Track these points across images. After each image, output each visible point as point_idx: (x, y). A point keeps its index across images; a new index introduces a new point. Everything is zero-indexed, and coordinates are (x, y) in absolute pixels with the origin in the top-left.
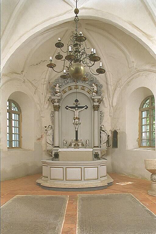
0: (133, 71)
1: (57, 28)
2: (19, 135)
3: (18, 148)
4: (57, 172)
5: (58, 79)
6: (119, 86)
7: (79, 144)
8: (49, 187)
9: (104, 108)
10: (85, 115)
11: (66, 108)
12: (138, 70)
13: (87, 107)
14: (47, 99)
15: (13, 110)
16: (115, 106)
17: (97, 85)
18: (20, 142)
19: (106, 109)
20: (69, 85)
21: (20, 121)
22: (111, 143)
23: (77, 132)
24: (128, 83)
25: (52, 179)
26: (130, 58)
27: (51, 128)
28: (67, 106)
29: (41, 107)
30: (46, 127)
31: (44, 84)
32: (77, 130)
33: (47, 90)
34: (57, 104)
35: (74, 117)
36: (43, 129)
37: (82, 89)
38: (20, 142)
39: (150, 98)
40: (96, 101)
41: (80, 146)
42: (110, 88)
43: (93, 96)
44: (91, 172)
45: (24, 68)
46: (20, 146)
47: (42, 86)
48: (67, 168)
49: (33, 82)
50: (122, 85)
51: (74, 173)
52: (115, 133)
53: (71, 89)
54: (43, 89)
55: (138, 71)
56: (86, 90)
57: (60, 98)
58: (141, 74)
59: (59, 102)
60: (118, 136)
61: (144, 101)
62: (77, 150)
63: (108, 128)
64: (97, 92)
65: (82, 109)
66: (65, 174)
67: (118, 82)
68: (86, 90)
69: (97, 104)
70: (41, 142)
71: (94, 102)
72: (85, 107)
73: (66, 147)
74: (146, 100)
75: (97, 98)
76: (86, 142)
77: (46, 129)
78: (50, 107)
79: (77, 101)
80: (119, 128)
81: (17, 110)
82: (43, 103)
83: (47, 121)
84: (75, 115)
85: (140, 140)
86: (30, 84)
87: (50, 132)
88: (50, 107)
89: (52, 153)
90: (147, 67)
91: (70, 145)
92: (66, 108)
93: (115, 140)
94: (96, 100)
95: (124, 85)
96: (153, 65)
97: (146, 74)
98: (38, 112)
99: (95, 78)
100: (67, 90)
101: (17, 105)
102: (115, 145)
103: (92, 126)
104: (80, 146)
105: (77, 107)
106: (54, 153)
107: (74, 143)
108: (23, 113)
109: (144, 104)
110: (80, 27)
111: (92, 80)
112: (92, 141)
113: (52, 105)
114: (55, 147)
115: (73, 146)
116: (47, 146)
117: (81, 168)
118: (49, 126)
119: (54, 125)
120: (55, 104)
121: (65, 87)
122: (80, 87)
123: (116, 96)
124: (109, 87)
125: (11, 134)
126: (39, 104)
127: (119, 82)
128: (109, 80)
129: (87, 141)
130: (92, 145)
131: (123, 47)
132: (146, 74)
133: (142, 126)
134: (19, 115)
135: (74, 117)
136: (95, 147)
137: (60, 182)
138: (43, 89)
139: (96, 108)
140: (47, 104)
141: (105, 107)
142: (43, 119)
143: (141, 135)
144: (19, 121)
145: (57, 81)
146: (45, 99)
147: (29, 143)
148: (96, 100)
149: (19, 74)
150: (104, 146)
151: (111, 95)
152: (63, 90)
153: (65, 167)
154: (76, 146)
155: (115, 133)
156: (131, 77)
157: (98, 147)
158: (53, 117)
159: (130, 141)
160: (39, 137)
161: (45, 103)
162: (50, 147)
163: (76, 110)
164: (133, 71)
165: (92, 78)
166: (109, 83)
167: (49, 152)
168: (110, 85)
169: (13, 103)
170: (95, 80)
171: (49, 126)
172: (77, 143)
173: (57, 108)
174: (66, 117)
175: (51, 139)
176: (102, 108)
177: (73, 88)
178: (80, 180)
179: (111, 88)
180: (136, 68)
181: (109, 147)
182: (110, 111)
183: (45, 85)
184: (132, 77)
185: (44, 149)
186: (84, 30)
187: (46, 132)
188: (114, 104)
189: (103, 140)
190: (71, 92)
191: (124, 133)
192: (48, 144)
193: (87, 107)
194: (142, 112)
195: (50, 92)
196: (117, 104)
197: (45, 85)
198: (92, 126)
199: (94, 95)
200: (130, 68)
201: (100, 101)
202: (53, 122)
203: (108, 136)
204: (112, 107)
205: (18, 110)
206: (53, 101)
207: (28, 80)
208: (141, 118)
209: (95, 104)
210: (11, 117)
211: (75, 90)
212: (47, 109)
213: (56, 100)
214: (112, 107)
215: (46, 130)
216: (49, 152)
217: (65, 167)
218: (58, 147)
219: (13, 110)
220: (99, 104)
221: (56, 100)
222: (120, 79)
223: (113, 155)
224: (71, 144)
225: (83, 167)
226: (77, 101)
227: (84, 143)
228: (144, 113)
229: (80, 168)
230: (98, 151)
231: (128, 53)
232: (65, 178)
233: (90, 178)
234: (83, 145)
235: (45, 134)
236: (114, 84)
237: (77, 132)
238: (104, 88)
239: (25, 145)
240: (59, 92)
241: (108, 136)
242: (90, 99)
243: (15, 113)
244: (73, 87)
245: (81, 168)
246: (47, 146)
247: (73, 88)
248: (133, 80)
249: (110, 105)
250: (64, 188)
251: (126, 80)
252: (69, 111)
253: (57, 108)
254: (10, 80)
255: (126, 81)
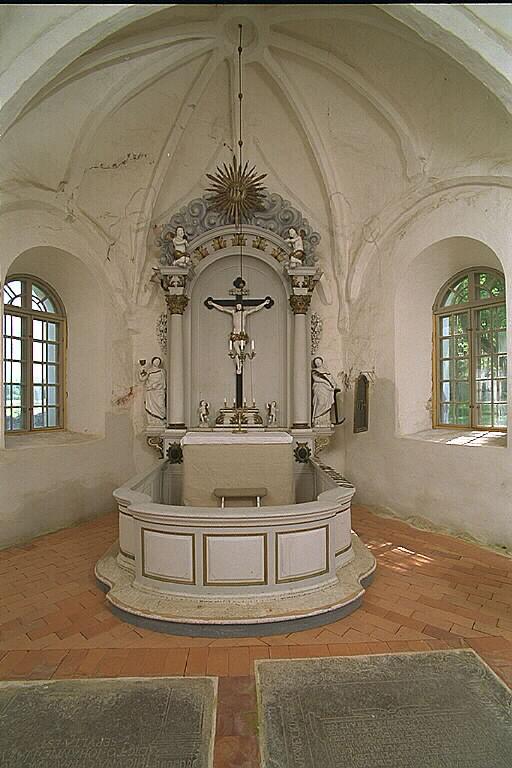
0: (420, 189)
1: (173, 40)
2: (58, 387)
3: (53, 428)
4: (170, 553)
5: (181, 215)
6: (371, 239)
7: (246, 415)
8: (136, 615)
9: (323, 306)
10: (266, 328)
11: (206, 303)
12: (441, 184)
13: (272, 302)
14: (146, 281)
15: (35, 307)
16: (359, 300)
17: (303, 235)
18: (60, 410)
19: (328, 308)
20: (217, 234)
21: (61, 344)
22: (348, 412)
23: (239, 378)
24: (402, 230)
25: (151, 577)
26: (414, 145)
27: (161, 365)
28: (210, 299)
29: (129, 301)
30: (143, 363)
31: (138, 231)
32: (239, 373)
33: (149, 248)
34: (179, 291)
35: (232, 334)
36: (134, 370)
37: (258, 248)
38: (60, 410)
39: (471, 275)
40: (301, 284)
41: (251, 422)
42: (342, 247)
43: (293, 268)
44: (303, 550)
45: (68, 172)
46: (61, 424)
47: (134, 235)
48: (209, 535)
49: (99, 222)
50: (382, 235)
51: (236, 554)
52: (363, 382)
53: (222, 244)
54: (136, 247)
55: (441, 187)
56: (270, 248)
57: (186, 272)
58: (449, 197)
59: (184, 285)
60: (370, 392)
61: (448, 283)
62: (240, 439)
63: (335, 361)
64: (303, 256)
65: (257, 308)
66: (202, 558)
67: (366, 226)
68: (270, 248)
69: (305, 292)
70: (129, 409)
71: (293, 286)
72: (263, 301)
73: (206, 425)
74: (456, 280)
75: (301, 272)
76: (270, 409)
77: (142, 368)
78: (156, 301)
79: (239, 283)
80: (371, 366)
81: (50, 310)
82: (135, 292)
83: (146, 344)
84: (234, 327)
85: (437, 405)
86: (92, 228)
87: (156, 378)
88: (156, 301)
89: (161, 444)
90: (477, 170)
91: (219, 420)
92: (206, 303)
93: (359, 406)
94: (301, 280)
95: (385, 236)
96: (500, 159)
97: (467, 195)
98: (120, 312)
99: (295, 214)
100: (209, 247)
101: (50, 293)
102: (361, 422)
103: (289, 359)
104: (251, 422)
105: (240, 302)
106: (167, 447)
107: (233, 415)
108: (73, 319)
109: (449, 292)
110: (253, 40)
111: (287, 220)
112: (289, 399)
113: (164, 293)
114: (172, 426)
115: (227, 422)
116: (146, 423)
117: (265, 535)
118: (155, 358)
119: (169, 358)
120: (173, 291)
121: (203, 239)
122: (249, 241)
123: (361, 268)
124: (340, 241)
125: (29, 388)
126: (121, 291)
127: (371, 226)
128: (339, 219)
129: (270, 406)
130: (289, 420)
131: (388, 109)
132: (467, 195)
133: (441, 362)
134: (58, 325)
135: (232, 334)
136: (295, 426)
137: (180, 593)
138: (134, 244)
139: (299, 305)
140: (148, 294)
141: (326, 303)
142: (134, 337)
143: (438, 387)
144: (58, 345)
145: (178, 221)
146: (141, 278)
147: (91, 413)
148: (301, 280)
149: (53, 190)
150: (324, 422)
151: (346, 260)
152: (198, 249)
153: (199, 534)
154: (239, 422)
155: (363, 382)
156: (411, 208)
157: (305, 426)
158: (165, 331)
159: (409, 405)
160: (122, 394)
161: (143, 289)
162: (156, 427)
163: (237, 311)
164: (420, 189)
165: (286, 212)
166: (339, 230)
167: (154, 442)
168: (342, 235)
169: (36, 285)
170: (296, 218)
171: (155, 358)
172: (239, 414)
173: (177, 305)
174: (209, 336)
175: (161, 402)
176: (315, 303)
177: (229, 243)
178: (261, 584)
179: (345, 245)
180: (431, 179)
181: (337, 423)
182: (342, 314)
183: (141, 234)
184: (412, 211)
185: (138, 430)
186: (267, 53)
187: (145, 378)
188: (355, 294)
189: (321, 403)
190: (221, 254)
191: (389, 385)
192: (149, 415)
193: (272, 302)
194: (441, 318)
195: (157, 255)
196: (364, 294)
197: (141, 234)
198: (289, 359)
199: (294, 265)
200: (409, 180)
201: (311, 283)
202: (166, 345)
203: (336, 391)
204: (349, 301)
205: (56, 310)
206: (165, 283)
207: (84, 214)
208: (438, 339)
209: (298, 292)
210: (29, 331)
211: (237, 250)
212: (148, 309)
213: (176, 279)
214: (349, 301)
215: (144, 372)
216: (154, 442)
217: (199, 534)
218: (182, 426)
219: (35, 307)
220: (310, 293)
221: (176, 279)
222: (374, 217)
223: (348, 450)
224: (222, 416)
225: (271, 532)
226: (239, 283)
227: (263, 414)
228: (446, 321)
229: (261, 534)
230: (307, 437)
231: (407, 132)
232: (202, 576)
233: (295, 573)
234: (258, 419)
235: (141, 386)
236: (354, 233)
237: (239, 378)
238: (323, 247)
239: (73, 420)
240: (185, 255)
241: (336, 391)
242: (282, 277)
243: (42, 317)
244: (229, 240)
245: (265, 535)
246: (146, 423)
247: (229, 243)
248: (419, 217)
249: (339, 296)
250: (196, 624)
251: (394, 218)
252: (217, 315)
253: (177, 305)
254: (18, 206)
255: (395, 221)
